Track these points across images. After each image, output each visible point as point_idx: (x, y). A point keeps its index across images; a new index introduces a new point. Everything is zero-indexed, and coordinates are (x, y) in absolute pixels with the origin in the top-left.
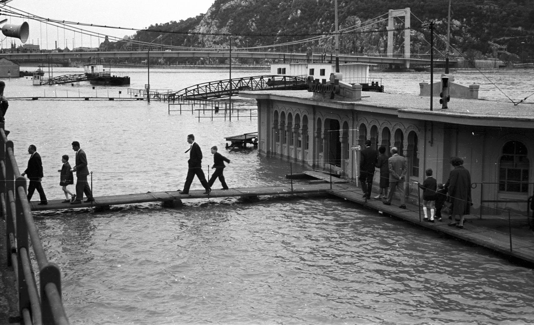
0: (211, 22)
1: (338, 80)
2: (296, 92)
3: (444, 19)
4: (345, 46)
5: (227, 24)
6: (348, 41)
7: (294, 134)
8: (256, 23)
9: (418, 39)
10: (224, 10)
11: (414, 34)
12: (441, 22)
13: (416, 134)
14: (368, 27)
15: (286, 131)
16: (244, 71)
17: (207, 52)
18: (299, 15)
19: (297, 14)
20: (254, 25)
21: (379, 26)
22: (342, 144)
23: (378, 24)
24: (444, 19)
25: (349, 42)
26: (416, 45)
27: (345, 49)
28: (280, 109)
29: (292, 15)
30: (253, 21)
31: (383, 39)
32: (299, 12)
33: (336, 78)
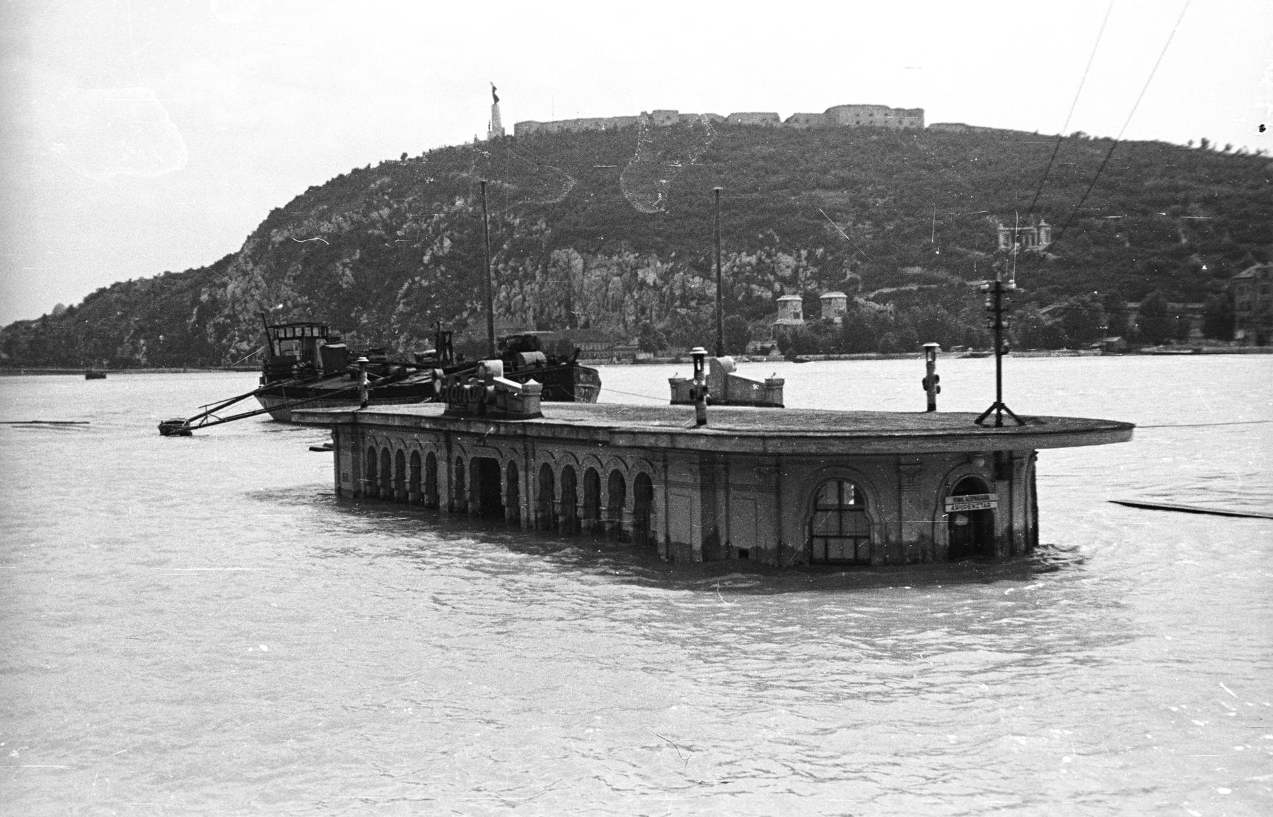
0: (252, 270)
1: (492, 376)
2: (1150, 519)
3: (759, 252)
4: (549, 314)
5: (289, 273)
6: (556, 304)
7: (469, 503)
8: (351, 269)
9: (706, 296)
10: (281, 243)
11: (697, 285)
12: (753, 259)
13: (597, 474)
14: (598, 273)
15: (393, 490)
16: (775, 434)
17: (925, 434)
18: (446, 251)
19: (442, 247)
20: (348, 272)
21: (622, 270)
22: (506, 509)
23: (619, 264)
24: (759, 252)
25: (559, 305)
26: (702, 308)
27: (551, 319)
28: (380, 440)
29: (432, 249)
30: (345, 265)
31: (633, 297)
32: (447, 243)
33: (489, 372)
